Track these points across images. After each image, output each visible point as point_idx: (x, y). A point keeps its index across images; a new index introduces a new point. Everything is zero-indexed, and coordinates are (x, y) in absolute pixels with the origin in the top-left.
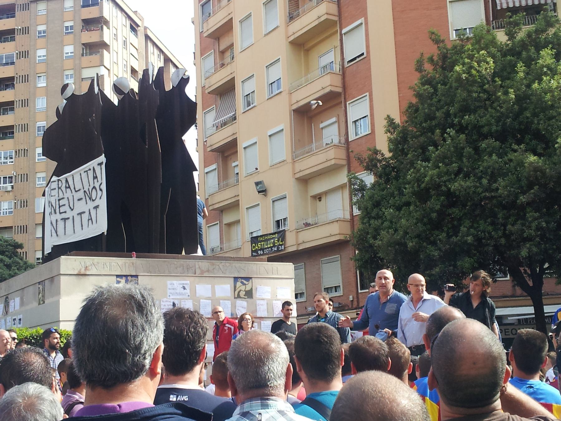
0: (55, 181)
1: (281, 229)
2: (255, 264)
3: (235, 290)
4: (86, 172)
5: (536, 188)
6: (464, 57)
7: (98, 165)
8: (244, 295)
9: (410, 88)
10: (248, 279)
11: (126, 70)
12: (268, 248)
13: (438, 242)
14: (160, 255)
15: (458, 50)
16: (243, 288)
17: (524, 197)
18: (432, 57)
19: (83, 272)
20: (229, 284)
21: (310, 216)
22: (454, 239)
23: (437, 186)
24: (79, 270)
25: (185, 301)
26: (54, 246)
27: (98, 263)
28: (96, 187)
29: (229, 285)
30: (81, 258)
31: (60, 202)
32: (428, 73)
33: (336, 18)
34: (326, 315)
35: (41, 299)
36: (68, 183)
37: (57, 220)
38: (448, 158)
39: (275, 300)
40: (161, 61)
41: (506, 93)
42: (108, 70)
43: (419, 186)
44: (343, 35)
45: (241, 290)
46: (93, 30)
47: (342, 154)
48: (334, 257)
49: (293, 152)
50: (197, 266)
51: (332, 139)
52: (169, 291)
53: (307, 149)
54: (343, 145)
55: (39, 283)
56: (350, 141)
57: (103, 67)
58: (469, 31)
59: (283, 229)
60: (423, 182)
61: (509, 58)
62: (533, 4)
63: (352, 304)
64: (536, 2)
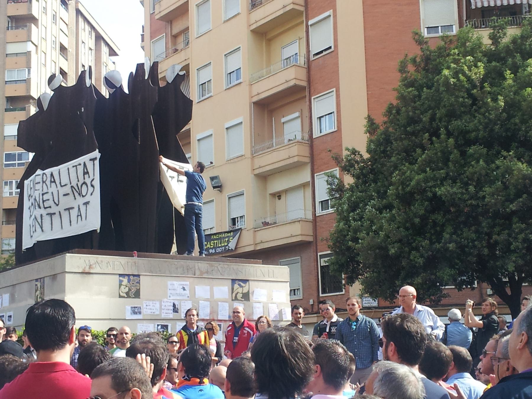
0: (40, 175)
1: (237, 228)
2: (252, 266)
3: (232, 293)
4: (75, 167)
5: (525, 196)
6: (450, 61)
7: (91, 160)
8: (241, 298)
9: (394, 90)
10: (245, 281)
11: (54, 46)
12: (222, 247)
13: (421, 248)
14: (159, 255)
15: (443, 52)
16: (240, 290)
17: (513, 206)
18: (415, 58)
19: (87, 270)
20: (209, 286)
21: (269, 216)
22: (438, 246)
23: (423, 192)
24: (83, 268)
25: (184, 302)
26: (38, 241)
27: (102, 261)
28: (87, 183)
29: (227, 287)
30: (85, 256)
31: (44, 196)
32: (411, 74)
33: (302, 9)
34: (357, 319)
35: (39, 297)
36: (53, 178)
37: (41, 215)
38: (434, 162)
39: (271, 303)
40: (92, 39)
41: (495, 100)
42: (36, 46)
43: (403, 189)
44: (310, 27)
45: (238, 293)
46: (20, 1)
47: (306, 151)
48: (294, 258)
49: (252, 147)
50: (197, 268)
51: (295, 135)
52: (169, 292)
53: (267, 144)
54: (307, 142)
55: (37, 280)
56: (314, 137)
57: (30, 42)
58: (441, 28)
59: (239, 227)
60: (408, 186)
61: (494, 64)
62: (509, 5)
63: (312, 308)
64: (512, 3)
